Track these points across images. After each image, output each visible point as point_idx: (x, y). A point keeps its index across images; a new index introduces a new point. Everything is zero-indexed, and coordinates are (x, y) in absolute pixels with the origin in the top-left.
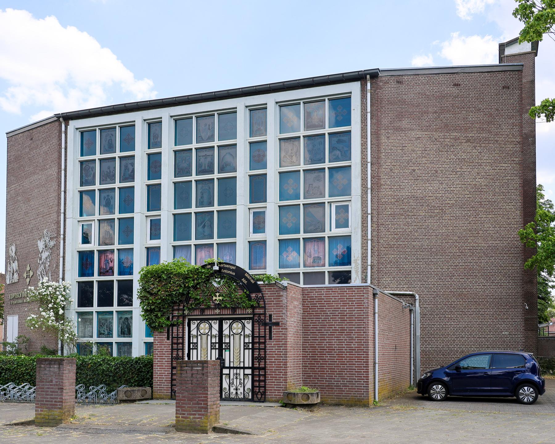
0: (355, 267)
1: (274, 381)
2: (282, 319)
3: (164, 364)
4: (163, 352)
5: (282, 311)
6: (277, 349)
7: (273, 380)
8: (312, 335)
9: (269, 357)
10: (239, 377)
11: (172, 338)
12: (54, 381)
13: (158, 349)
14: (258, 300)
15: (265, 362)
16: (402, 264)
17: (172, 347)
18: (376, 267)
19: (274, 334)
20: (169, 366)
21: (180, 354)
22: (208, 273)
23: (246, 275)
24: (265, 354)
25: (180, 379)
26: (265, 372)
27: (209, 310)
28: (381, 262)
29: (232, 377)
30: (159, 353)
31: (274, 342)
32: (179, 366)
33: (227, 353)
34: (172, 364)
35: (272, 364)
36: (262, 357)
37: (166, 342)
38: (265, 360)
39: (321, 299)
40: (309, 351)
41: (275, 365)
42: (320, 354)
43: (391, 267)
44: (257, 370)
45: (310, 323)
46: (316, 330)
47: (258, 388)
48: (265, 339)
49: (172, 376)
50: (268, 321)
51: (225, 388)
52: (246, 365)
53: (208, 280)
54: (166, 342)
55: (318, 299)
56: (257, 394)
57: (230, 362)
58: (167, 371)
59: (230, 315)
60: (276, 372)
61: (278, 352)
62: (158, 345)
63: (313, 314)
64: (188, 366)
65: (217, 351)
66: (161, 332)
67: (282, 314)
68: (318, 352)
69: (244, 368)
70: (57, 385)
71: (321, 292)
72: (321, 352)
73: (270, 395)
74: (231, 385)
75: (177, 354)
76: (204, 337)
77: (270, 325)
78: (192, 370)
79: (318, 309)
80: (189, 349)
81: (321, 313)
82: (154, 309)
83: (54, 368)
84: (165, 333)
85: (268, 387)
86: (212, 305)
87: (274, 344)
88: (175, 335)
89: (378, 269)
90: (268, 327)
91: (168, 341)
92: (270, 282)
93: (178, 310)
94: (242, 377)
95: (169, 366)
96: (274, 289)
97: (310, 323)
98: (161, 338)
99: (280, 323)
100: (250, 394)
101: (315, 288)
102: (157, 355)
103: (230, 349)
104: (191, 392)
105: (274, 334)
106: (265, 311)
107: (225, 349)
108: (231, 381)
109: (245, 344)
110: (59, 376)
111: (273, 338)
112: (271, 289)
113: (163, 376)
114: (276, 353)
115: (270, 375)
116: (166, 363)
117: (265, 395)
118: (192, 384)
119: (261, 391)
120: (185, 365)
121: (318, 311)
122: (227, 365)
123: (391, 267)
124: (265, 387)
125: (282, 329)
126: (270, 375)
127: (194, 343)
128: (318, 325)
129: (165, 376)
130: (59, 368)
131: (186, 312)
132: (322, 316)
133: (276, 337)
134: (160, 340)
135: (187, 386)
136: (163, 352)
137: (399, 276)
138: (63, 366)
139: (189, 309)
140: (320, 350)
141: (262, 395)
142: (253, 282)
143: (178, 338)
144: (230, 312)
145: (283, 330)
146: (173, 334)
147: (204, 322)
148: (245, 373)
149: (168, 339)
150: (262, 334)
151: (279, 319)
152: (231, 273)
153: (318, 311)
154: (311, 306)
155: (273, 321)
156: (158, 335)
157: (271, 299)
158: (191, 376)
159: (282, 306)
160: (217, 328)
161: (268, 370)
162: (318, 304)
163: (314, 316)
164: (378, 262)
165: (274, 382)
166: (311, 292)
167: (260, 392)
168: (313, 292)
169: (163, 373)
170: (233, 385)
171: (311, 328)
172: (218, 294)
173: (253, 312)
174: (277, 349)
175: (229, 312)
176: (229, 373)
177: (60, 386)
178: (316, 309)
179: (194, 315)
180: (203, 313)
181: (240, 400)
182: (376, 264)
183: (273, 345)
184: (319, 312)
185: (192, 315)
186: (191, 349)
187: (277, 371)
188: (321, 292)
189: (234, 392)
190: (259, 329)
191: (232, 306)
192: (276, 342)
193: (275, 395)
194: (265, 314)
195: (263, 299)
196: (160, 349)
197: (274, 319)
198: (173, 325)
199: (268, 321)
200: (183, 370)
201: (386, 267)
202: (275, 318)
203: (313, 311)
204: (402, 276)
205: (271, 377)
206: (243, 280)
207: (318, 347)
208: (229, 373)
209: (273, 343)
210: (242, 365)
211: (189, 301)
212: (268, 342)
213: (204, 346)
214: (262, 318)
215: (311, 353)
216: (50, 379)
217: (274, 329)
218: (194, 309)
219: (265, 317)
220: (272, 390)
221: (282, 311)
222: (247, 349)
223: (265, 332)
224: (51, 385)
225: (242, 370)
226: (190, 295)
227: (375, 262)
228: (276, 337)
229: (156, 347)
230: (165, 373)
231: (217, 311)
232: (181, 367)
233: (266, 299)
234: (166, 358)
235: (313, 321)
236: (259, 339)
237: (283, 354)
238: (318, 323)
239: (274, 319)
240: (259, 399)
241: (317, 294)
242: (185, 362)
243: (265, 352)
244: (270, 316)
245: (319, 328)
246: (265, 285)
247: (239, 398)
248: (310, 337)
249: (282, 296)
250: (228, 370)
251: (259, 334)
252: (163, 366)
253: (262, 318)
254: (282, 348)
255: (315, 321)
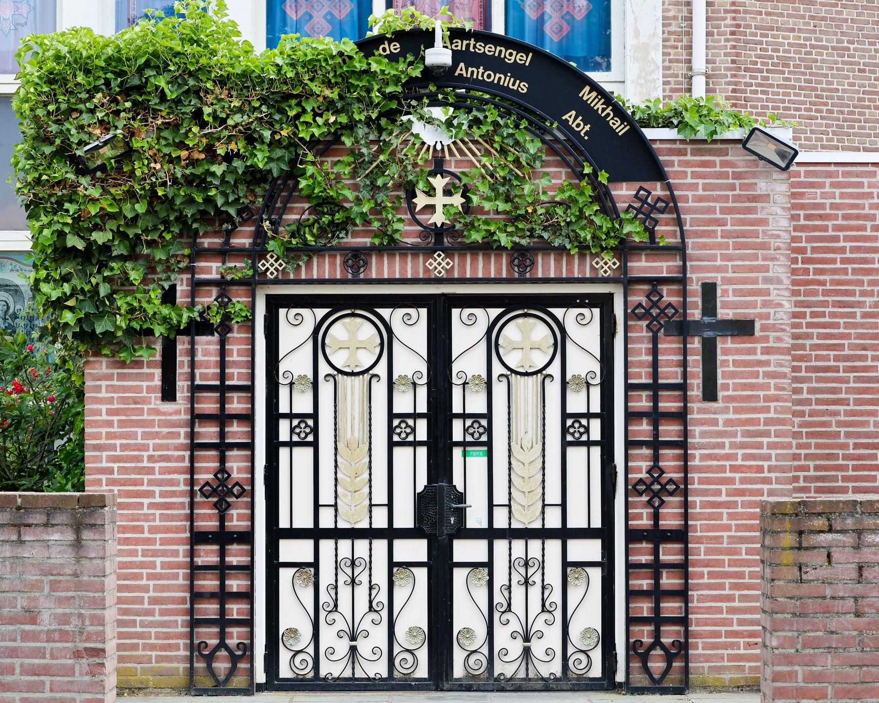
0: (639, 77)
1: (727, 592)
2: (765, 304)
3: (146, 518)
4: (139, 459)
5: (766, 269)
6: (743, 446)
7: (721, 587)
8: (819, 380)
9: (701, 481)
10: (537, 578)
11: (195, 389)
12: (45, 616)
13: (113, 447)
14: (648, 216)
15: (686, 505)
16: (826, 76)
17: (192, 435)
18: (728, 83)
19: (725, 375)
20: (177, 530)
21: (236, 465)
22: (397, 80)
23: (586, 94)
24: (685, 469)
25: (797, 593)
26: (686, 552)
27: (487, 257)
28: (745, 62)
29: (500, 578)
30: (116, 466)
31: (726, 410)
32: (788, 525)
33: (477, 462)
34: (191, 518)
35: (719, 516)
36: (671, 481)
37: (157, 412)
38: (685, 493)
39: (858, 217)
40: (803, 452)
41: (731, 516)
42: (856, 468)
43: (786, 87)
44: (644, 545)
45: (810, 325)
46: (837, 358)
47: (648, 628)
48: (685, 399)
49: (192, 577)
50: (695, 314)
51: (468, 630)
52: (576, 521)
53: (391, 115)
54: (157, 412)
55: (846, 217)
56: (210, 659)
57: (317, 506)
58: (164, 553)
59: (498, 281)
60: (737, 552)
61: (746, 457)
62: (110, 424)
63: (823, 283)
64: (837, 526)
65: (422, 452)
66: (123, 364)
67: (767, 280)
68: (846, 457)
69: (565, 534)
70: (64, 636)
71: (860, 185)
72: (860, 457)
73: (708, 659)
74: (496, 616)
75: (222, 469)
76: (353, 387)
77: (708, 334)
78: (857, 547)
79: (844, 261)
80: (273, 445)
81: (860, 283)
82: (106, 248)
83: (46, 544)
84: (150, 364)
85: (699, 623)
86: (408, 234)
87: (728, 423)
88: (204, 376)
89: (734, 91)
90: (696, 344)
91: (168, 407)
92: (715, 132)
93: (224, 253)
94: (554, 575)
95: (177, 530)
96: (724, 164)
97: (810, 325)
98: (125, 389)
99: (757, 326)
100: (423, 655)
101: (832, 168)
102: (104, 477)
103: (489, 444)
104: (854, 653)
105: (150, 377)
106: (684, 269)
107: (464, 444)
108: (498, 598)
109: (396, 422)
110: (79, 587)
111: (721, 394)
112: (713, 164)
113: (138, 577)
114: (739, 462)
115: (707, 564)
116: (158, 512)
117: (686, 659)
118: (858, 615)
119: (666, 641)
120: (819, 523)
121: (845, 271)
122: (476, 519)
123: (786, 87)
124: (684, 621)
125: (767, 351)
126: (707, 564)
127: (297, 416)
128: (847, 336)
129: (151, 577)
130: (78, 544)
131: (270, 266)
132: (863, 293)
133: (736, 387)
134: (123, 400)
135: (833, 625)
136: (139, 459)
137: (816, 125)
138: (103, 532)
139: (291, 253)
140: (856, 446)
141: (669, 658)
142: (619, 128)
143: (655, 388)
144: (499, 270)
145: (772, 358)
146: (197, 372)
147: (353, 315)
148: (570, 559)
149: (168, 393)
150: (670, 374)
151: (754, 305)
152: (507, 81)
153: (845, 271)
154: (814, 250)
155: (724, 313)
156: (110, 377)
157: (712, 210)
158: (854, 575)
159: (764, 246)
160: (422, 347)
161: (699, 540)
162: (847, 239)
163: (826, 293)
164: (733, 62)
165: (730, 598)
166: (812, 185)
167: (227, 648)
168: (821, 185)
169: (142, 565)
170: (508, 616)
171: (814, 347)
172: (439, 183)
173: (624, 268)
174: (743, 446)
175: (497, 267)
176: (311, 559)
177: (88, 639)
178: (834, 261)
179: (310, 282)
180: (356, 272)
181: (547, 685)
182: (726, 69)
183: (721, 428)
184: (850, 277)
185: (298, 282)
186: (285, 444)
187: (744, 546)
188: (860, 185)
189: (516, 648)
190: (655, 352)
191: (517, 240)
192: (736, 411)
193: (732, 658)
194: (682, 281)
195: (676, 210)
196: (124, 447)
197: (725, 305)
198: (200, 327)
199: (695, 314)
200: (807, 549)
201: (765, 85)
202: (731, 298)
203: (822, 272)
204: (827, 126)
205: (711, 575)
206: (570, 116)
207: (848, 435)
208: (311, 559)
209: (721, 418)
210: (553, 521)
211: (285, 210)
212: (697, 409)
213: (353, 429)
214: (666, 299)
215: (812, 464)
216: (21, 602)
217: (726, 352)
218: (310, 252)
219: (684, 293)
220: (717, 634)
221: (766, 269)
222: (577, 443)
223: (684, 364)
224: (26, 636)
225: (554, 546)
226: (303, 183)
227: (723, 62)
228: (736, 387)
229: (98, 436)
230: (153, 565)
231: (439, 264)
232: (801, 533)
233: (689, 211)
234: (157, 489)
235: (823, 315)
236: (655, 399)
237: (771, 469)
238: (847, 325)
239: (725, 305)
240: (657, 676)
241: (842, 196)
242: (819, 509)
243: (685, 458)
244: (709, 291)
245: (852, 347)
246: (677, 148)
247: (543, 679)
248: (811, 391)
249: (765, 198)
250: (310, 543)
251: (655, 375)
252: (140, 530)
253: (666, 299)
254: (765, 440)
255: (833, 315)
